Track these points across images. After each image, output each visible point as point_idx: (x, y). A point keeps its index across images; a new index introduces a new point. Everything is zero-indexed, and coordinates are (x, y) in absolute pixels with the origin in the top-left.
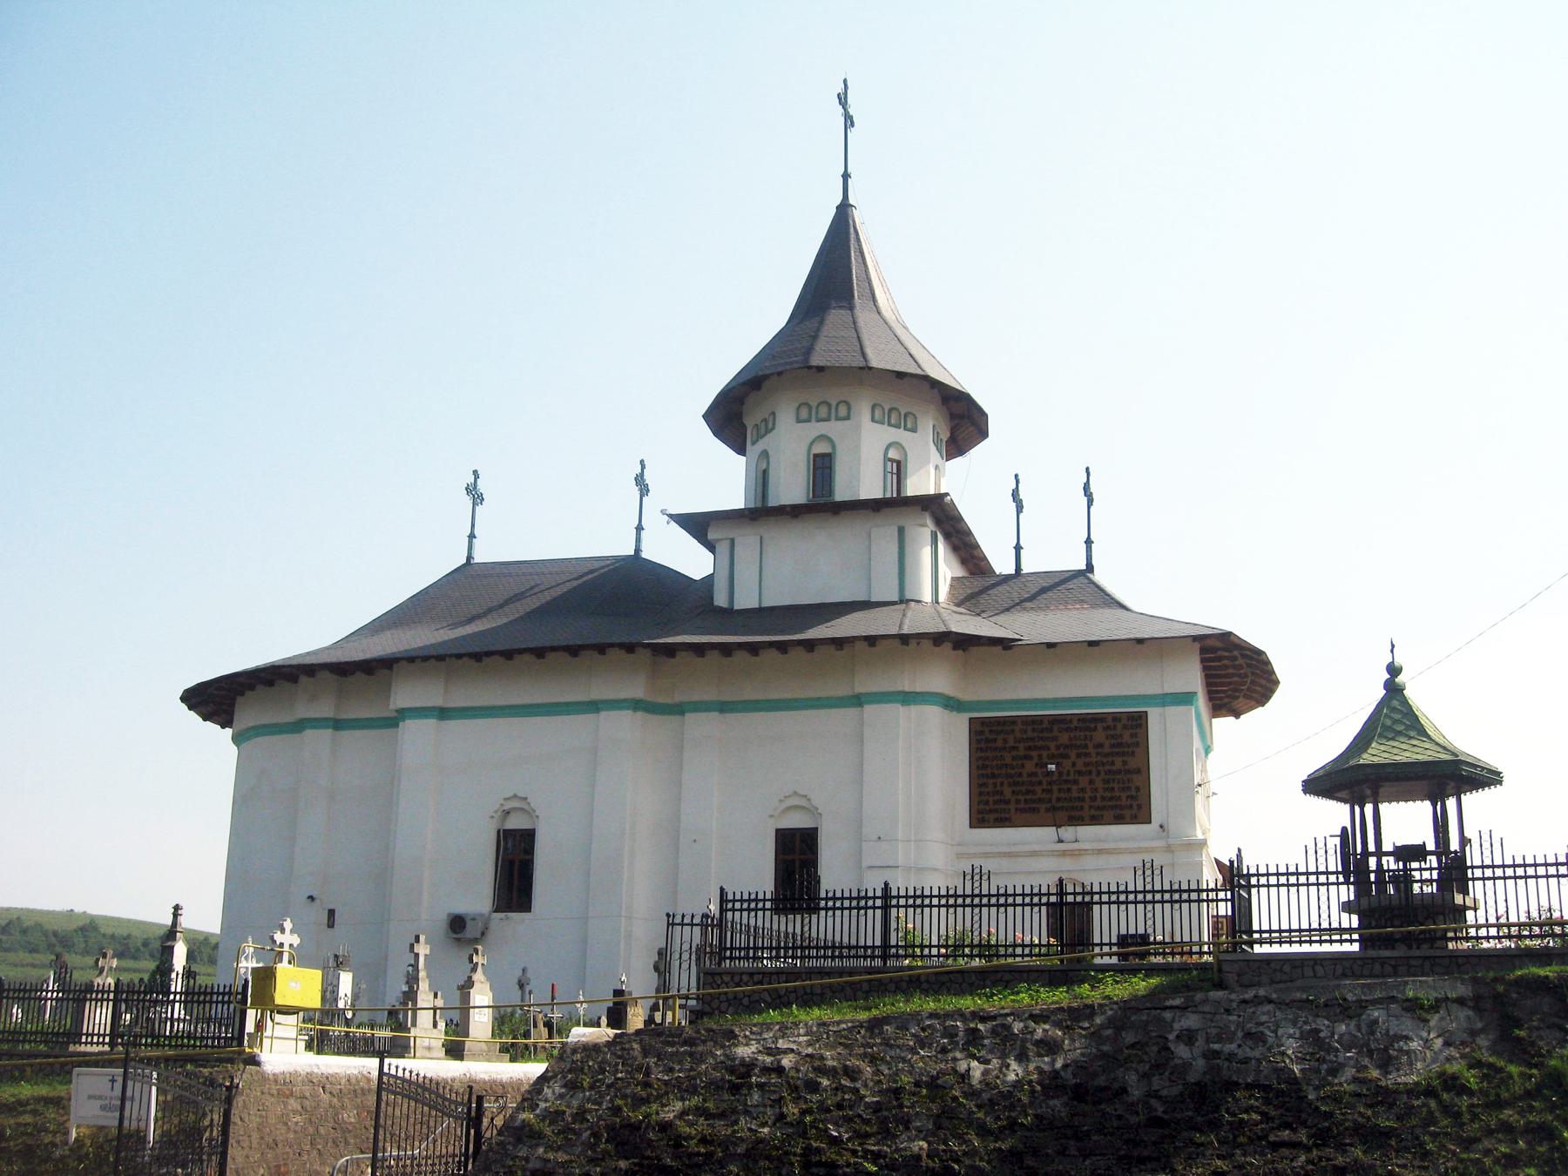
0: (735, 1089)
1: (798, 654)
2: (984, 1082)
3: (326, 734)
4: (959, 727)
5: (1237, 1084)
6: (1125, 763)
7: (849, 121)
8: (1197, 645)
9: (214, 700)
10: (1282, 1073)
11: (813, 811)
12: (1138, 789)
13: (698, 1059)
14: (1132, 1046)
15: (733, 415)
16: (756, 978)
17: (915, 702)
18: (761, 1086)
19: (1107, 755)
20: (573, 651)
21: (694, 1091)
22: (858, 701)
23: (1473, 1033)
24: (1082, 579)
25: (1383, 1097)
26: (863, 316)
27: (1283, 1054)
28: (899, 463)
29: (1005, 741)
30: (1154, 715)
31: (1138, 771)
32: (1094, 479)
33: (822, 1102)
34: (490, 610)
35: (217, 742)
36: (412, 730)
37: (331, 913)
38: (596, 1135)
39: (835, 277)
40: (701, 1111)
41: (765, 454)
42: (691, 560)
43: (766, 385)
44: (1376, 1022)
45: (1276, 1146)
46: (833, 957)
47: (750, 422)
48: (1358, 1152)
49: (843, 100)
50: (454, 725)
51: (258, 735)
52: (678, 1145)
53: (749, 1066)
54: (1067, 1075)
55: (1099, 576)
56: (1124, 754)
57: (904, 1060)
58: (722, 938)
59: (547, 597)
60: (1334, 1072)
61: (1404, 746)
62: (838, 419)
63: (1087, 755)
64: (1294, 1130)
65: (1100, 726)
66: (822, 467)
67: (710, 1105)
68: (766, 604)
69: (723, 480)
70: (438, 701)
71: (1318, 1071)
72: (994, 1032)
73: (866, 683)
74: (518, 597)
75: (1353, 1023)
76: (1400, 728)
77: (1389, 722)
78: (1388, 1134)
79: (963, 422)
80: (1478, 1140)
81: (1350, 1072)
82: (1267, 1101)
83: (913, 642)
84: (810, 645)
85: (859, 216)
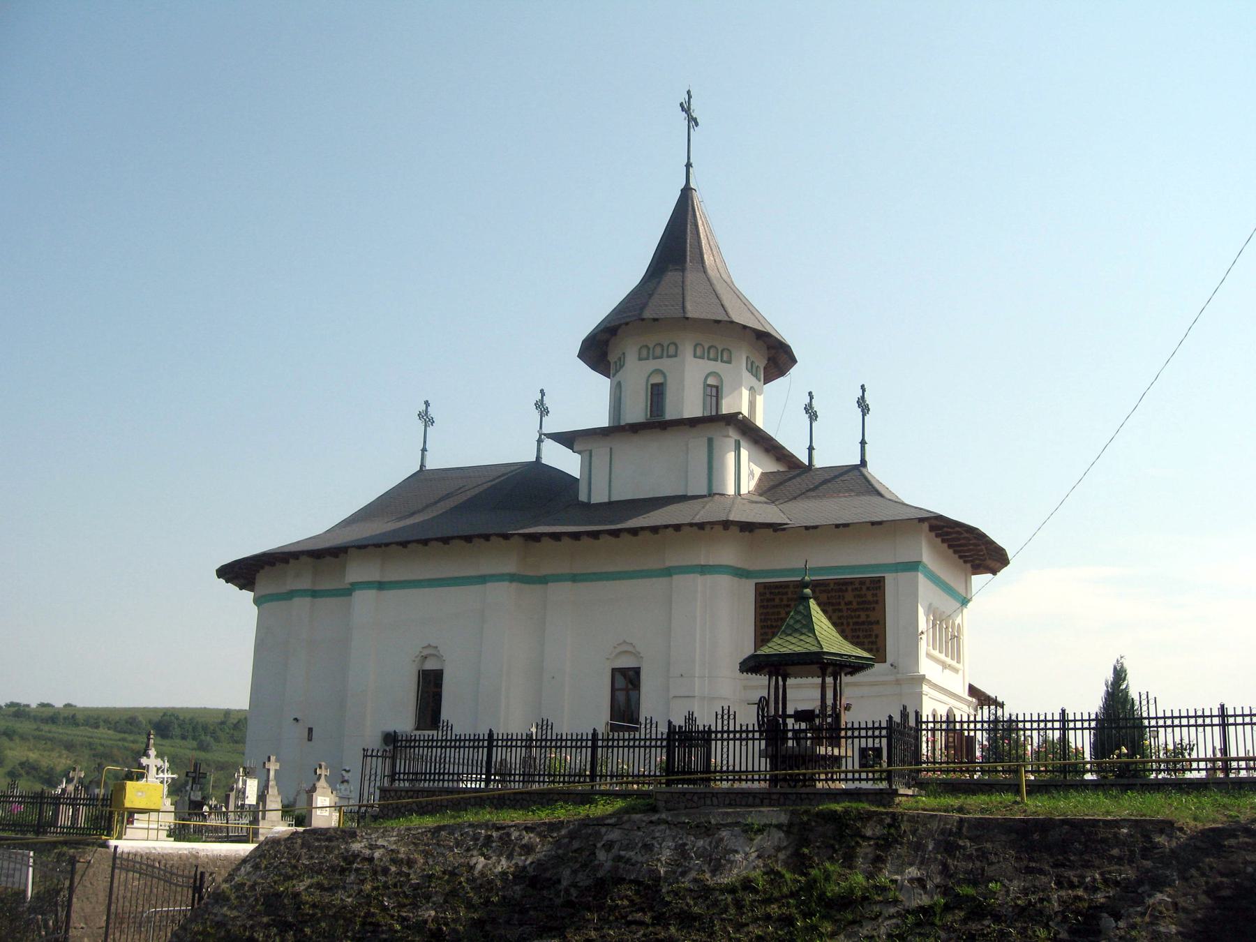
0: (343, 871)
1: (626, 537)
2: (482, 873)
3: (307, 600)
4: (748, 590)
5: (624, 879)
6: (868, 616)
7: (692, 121)
8: (926, 526)
9: (240, 573)
10: (653, 873)
11: (636, 655)
12: (877, 636)
13: (329, 850)
14: (575, 851)
15: (599, 350)
16: (410, 794)
17: (710, 573)
18: (357, 870)
19: (856, 610)
20: (468, 539)
21: (319, 872)
22: (668, 572)
23: (779, 849)
24: (856, 473)
25: (704, 892)
26: (691, 276)
27: (659, 860)
28: (717, 387)
29: (781, 600)
30: (890, 579)
31: (878, 622)
32: (875, 389)
33: (386, 882)
34: (427, 507)
35: (241, 605)
36: (358, 595)
37: (310, 730)
38: (257, 900)
39: (679, 245)
40: (319, 886)
41: (619, 384)
42: (567, 461)
43: (620, 331)
44: (722, 840)
45: (629, 924)
46: (434, 780)
47: (612, 358)
48: (673, 930)
49: (686, 108)
50: (389, 594)
51: (272, 600)
52: (299, 908)
53: (356, 856)
54: (530, 870)
55: (875, 470)
56: (867, 609)
57: (443, 855)
58: (394, 766)
59: (470, 494)
60: (683, 874)
61: (794, 641)
62: (668, 356)
63: (840, 610)
64: (645, 914)
65: (850, 588)
66: (657, 393)
67: (325, 882)
68: (613, 499)
70: (376, 576)
71: (675, 872)
72: (501, 838)
73: (673, 559)
74: (448, 496)
75: (708, 840)
76: (797, 626)
77: (792, 622)
78: (698, 917)
80: (747, 925)
81: (693, 874)
82: (637, 892)
83: (708, 528)
84: (634, 532)
85: (698, 197)
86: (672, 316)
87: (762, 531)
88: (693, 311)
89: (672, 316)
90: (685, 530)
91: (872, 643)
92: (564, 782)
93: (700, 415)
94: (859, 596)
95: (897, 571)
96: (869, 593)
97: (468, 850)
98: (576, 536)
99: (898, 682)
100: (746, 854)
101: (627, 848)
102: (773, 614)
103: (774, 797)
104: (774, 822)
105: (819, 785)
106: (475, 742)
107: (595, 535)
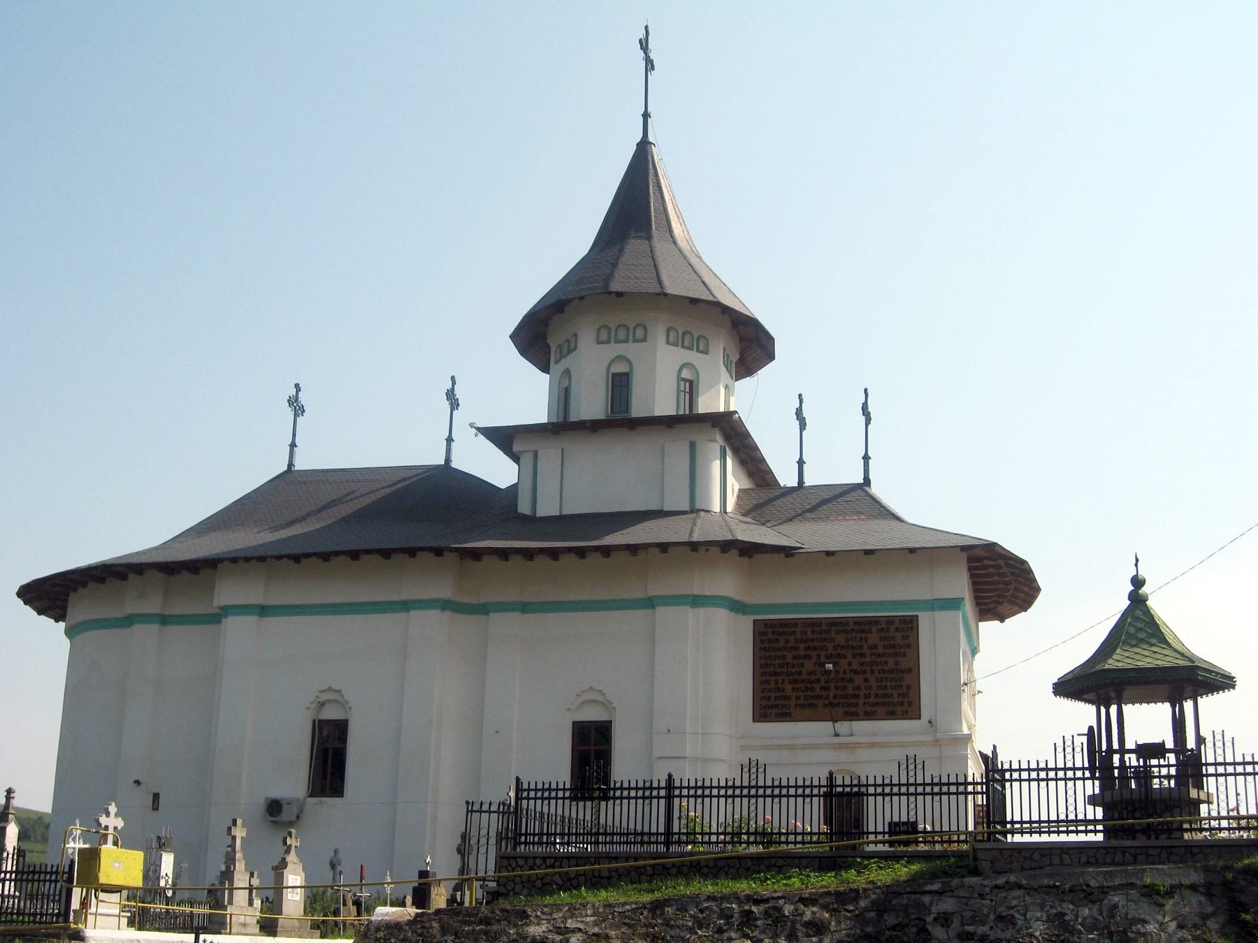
1: (596, 558)
4: (745, 625)
6: (897, 663)
7: (649, 65)
9: (48, 595)
11: (606, 705)
12: (909, 687)
14: (894, 928)
15: (538, 336)
17: (703, 605)
20: (386, 553)
22: (650, 603)
23: (1205, 917)
24: (859, 492)
27: (1031, 935)
28: (691, 382)
29: (787, 641)
30: (924, 620)
31: (910, 670)
36: (233, 624)
37: (156, 796)
39: (636, 207)
41: (567, 373)
47: (554, 342)
55: (876, 489)
56: (896, 654)
59: (365, 501)
61: (1146, 653)
62: (635, 341)
63: (862, 655)
65: (874, 628)
66: (620, 385)
68: (565, 512)
69: (527, 395)
72: (766, 914)
75: (1095, 908)
76: (1142, 635)
77: (1132, 631)
79: (751, 345)
85: (657, 153)
86: (626, 296)
87: (768, 556)
88: (672, 288)
89: (626, 296)
90: (673, 551)
91: (903, 695)
92: (803, 843)
93: (672, 412)
94: (885, 638)
95: (933, 609)
96: (899, 636)
97: (720, 931)
98: (528, 554)
99: (937, 743)
100: (1161, 924)
101: (973, 921)
102: (776, 657)
103: (1152, 852)
104: (1186, 882)
105: (1186, 836)
106: (646, 792)
107: (554, 554)
